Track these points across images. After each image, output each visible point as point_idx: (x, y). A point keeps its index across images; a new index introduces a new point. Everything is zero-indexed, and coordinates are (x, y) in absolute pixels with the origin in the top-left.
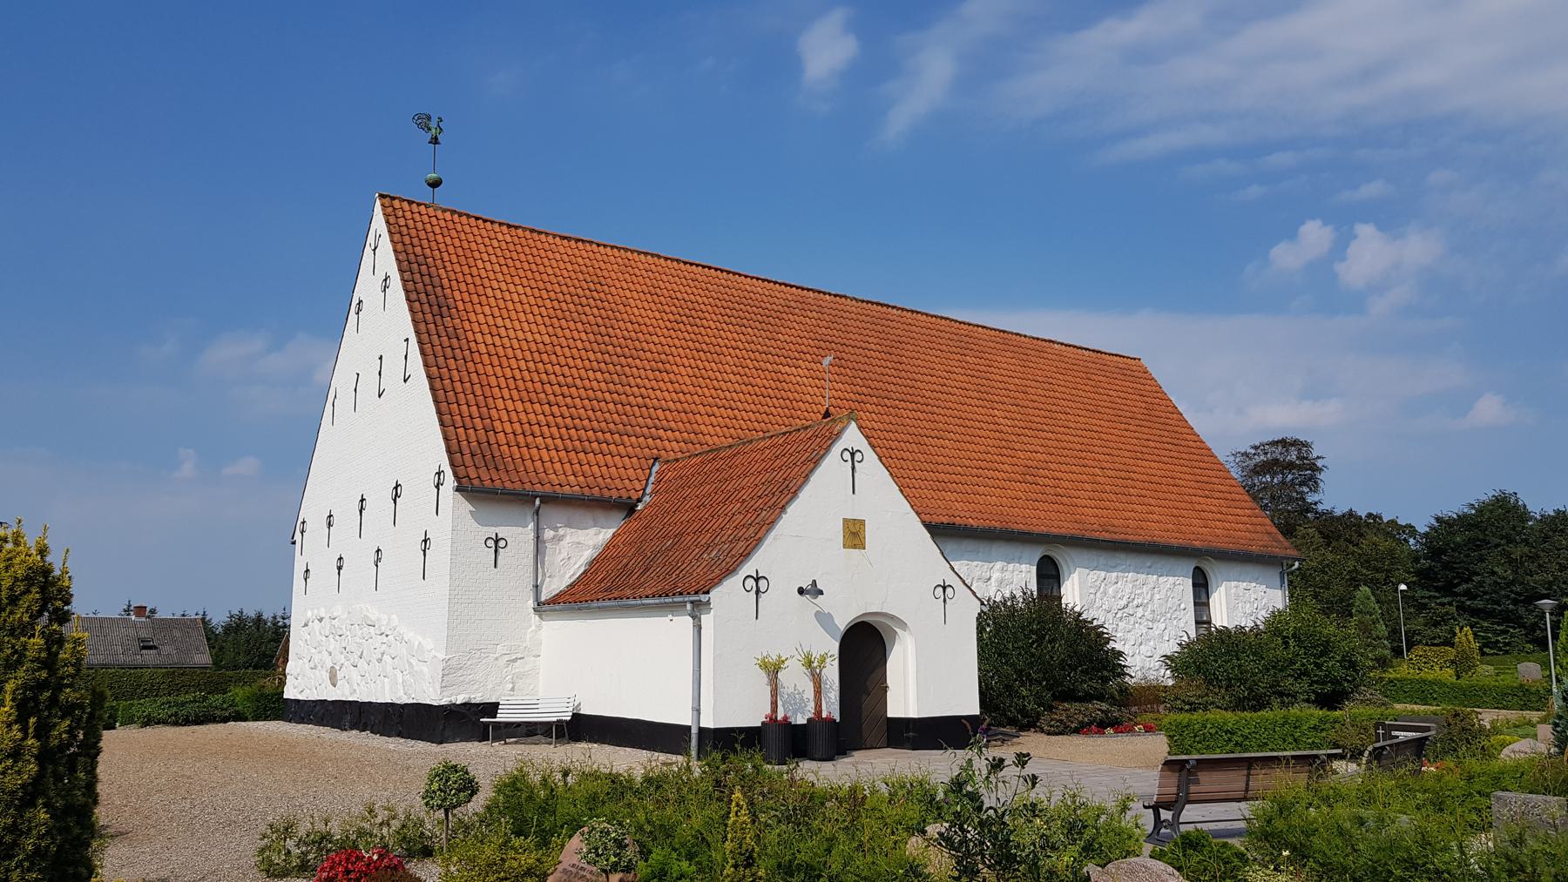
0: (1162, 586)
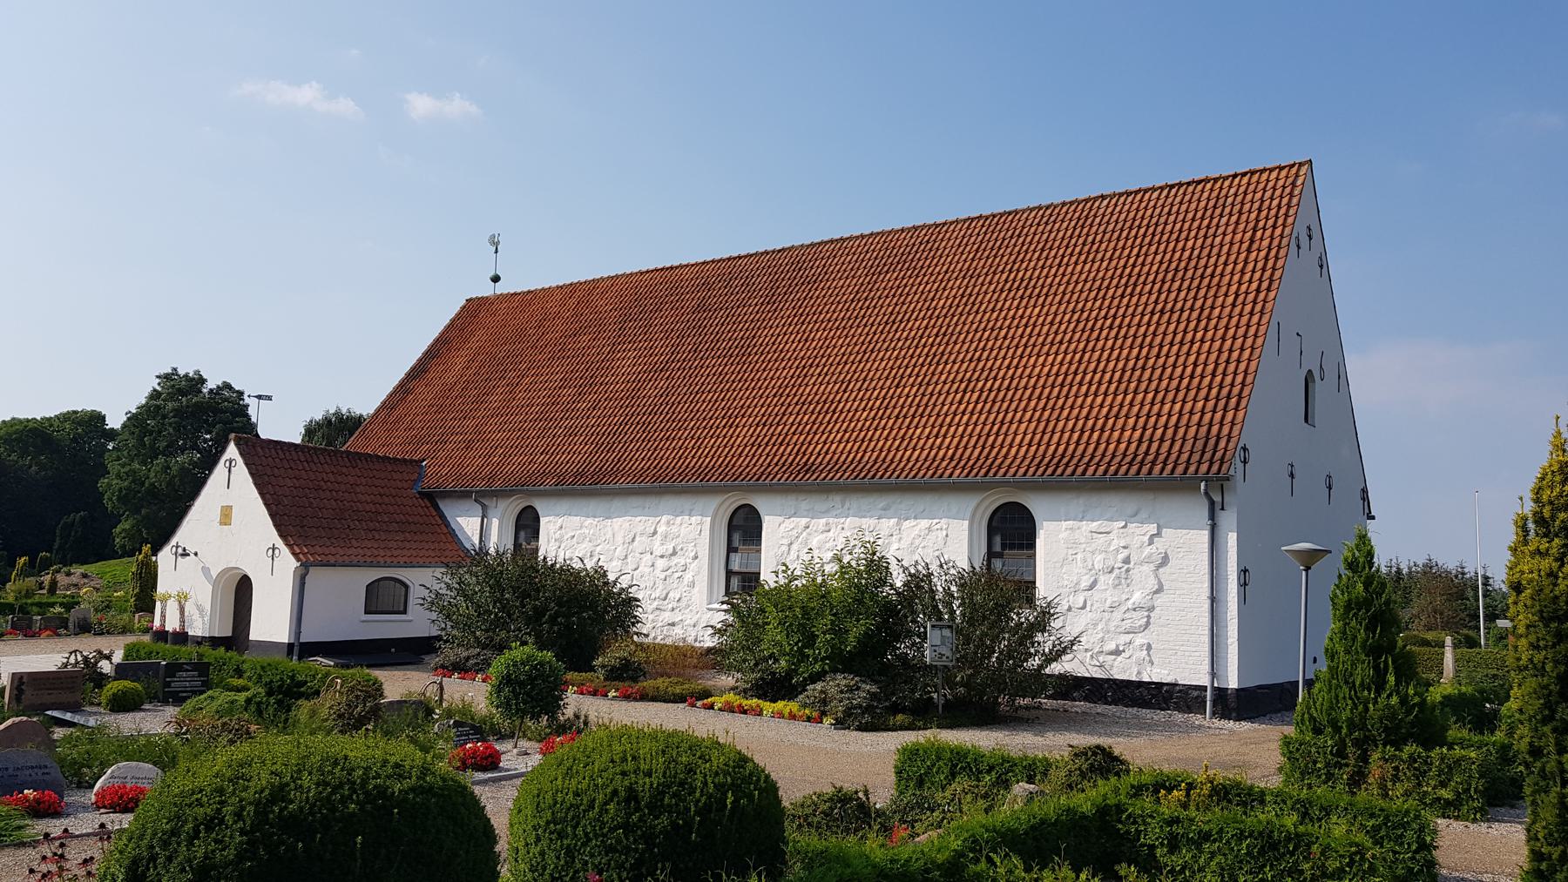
0: (904, 534)
